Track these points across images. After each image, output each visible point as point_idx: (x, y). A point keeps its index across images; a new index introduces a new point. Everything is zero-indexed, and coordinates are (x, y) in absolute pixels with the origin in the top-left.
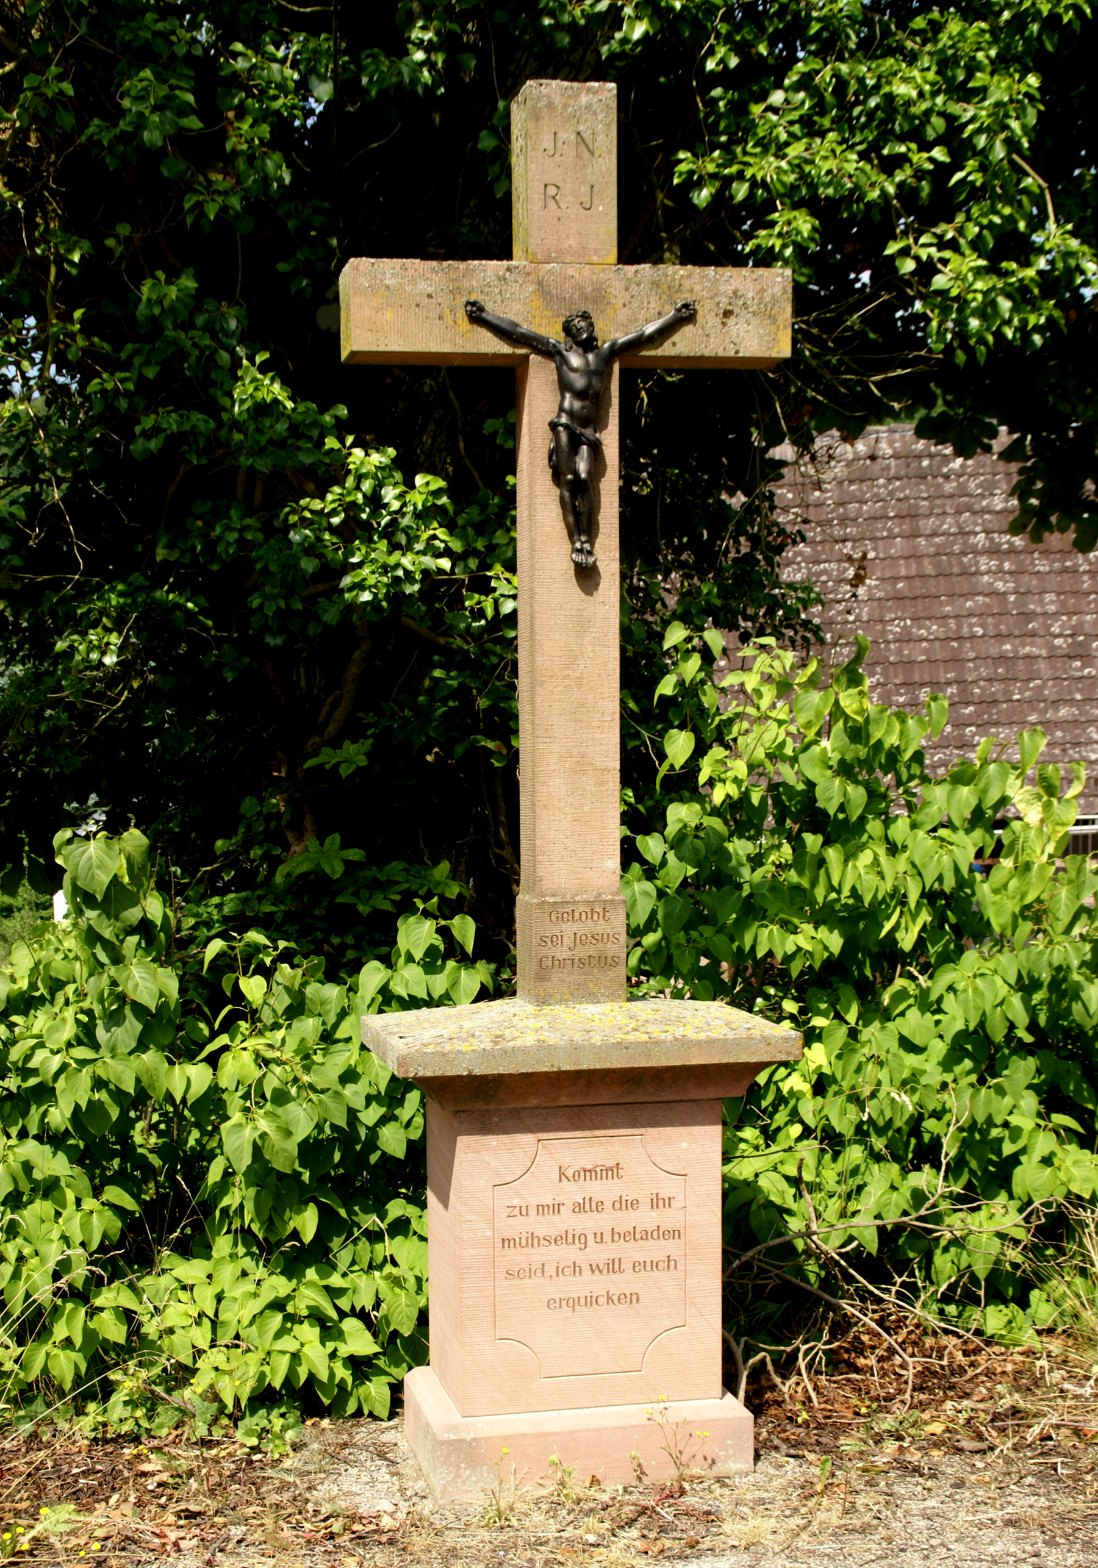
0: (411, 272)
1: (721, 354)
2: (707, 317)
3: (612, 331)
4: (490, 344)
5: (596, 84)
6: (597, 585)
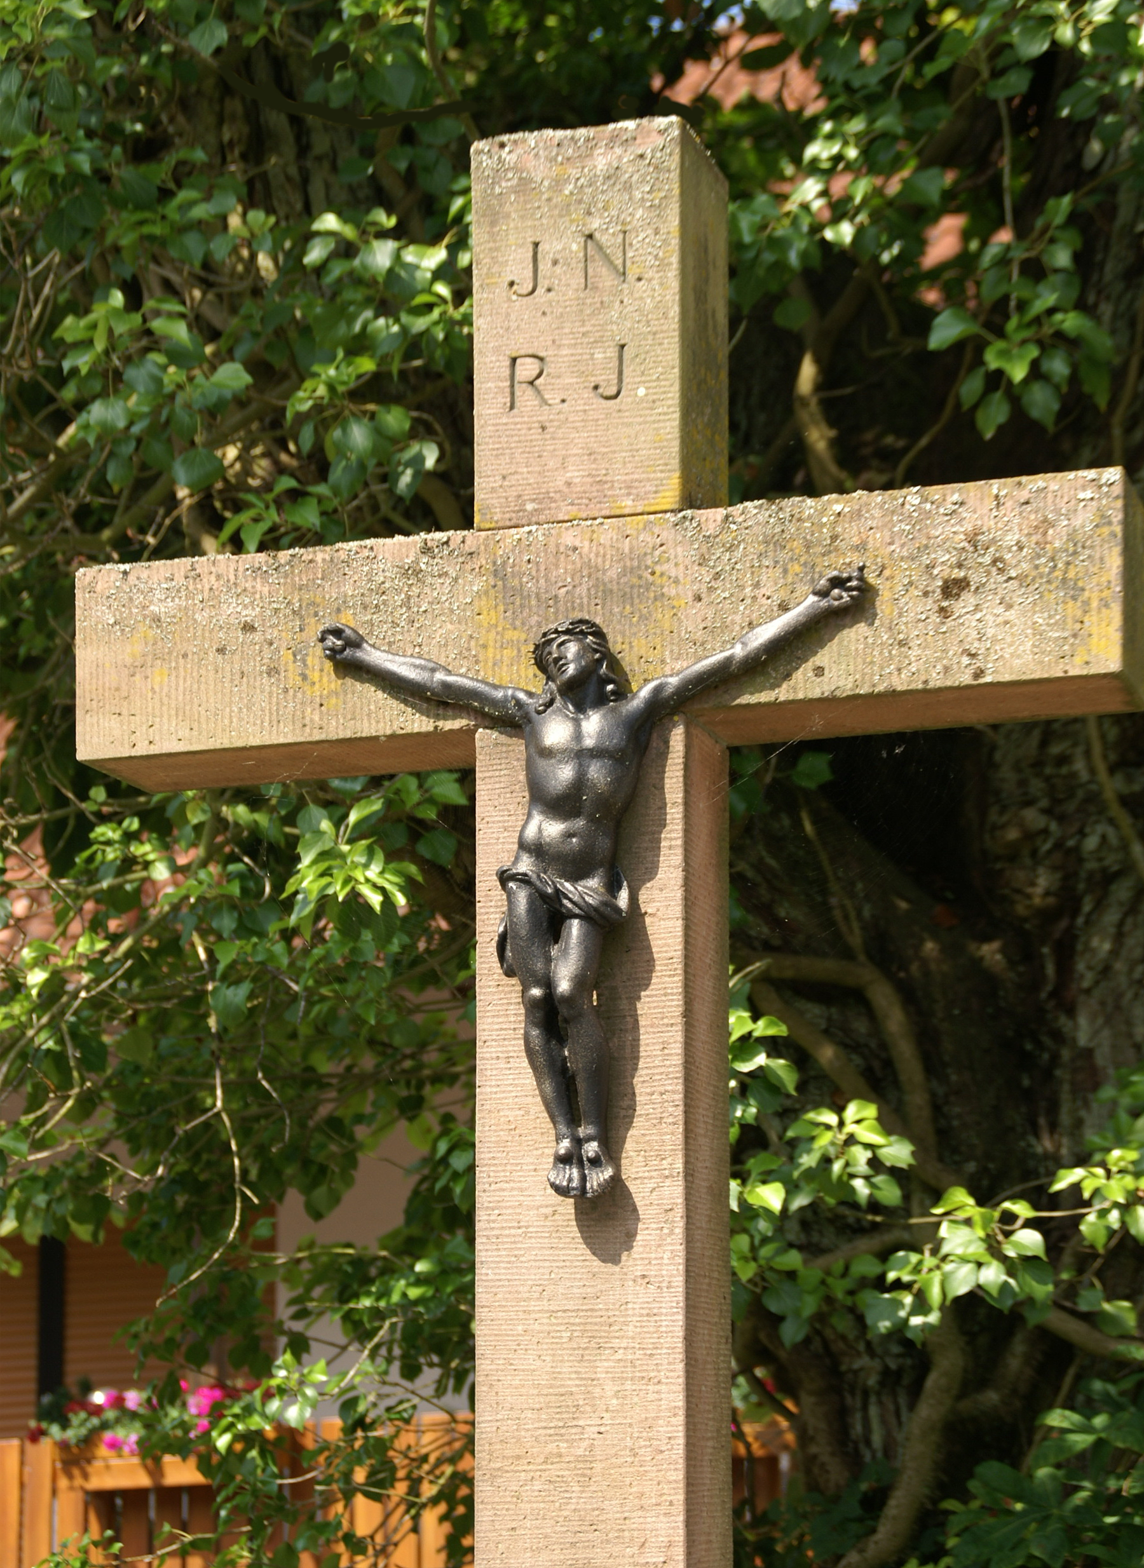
0: (209, 581)
1: (937, 681)
2: (902, 603)
3: (659, 662)
4: (382, 717)
5: (630, 124)
6: (631, 1236)
